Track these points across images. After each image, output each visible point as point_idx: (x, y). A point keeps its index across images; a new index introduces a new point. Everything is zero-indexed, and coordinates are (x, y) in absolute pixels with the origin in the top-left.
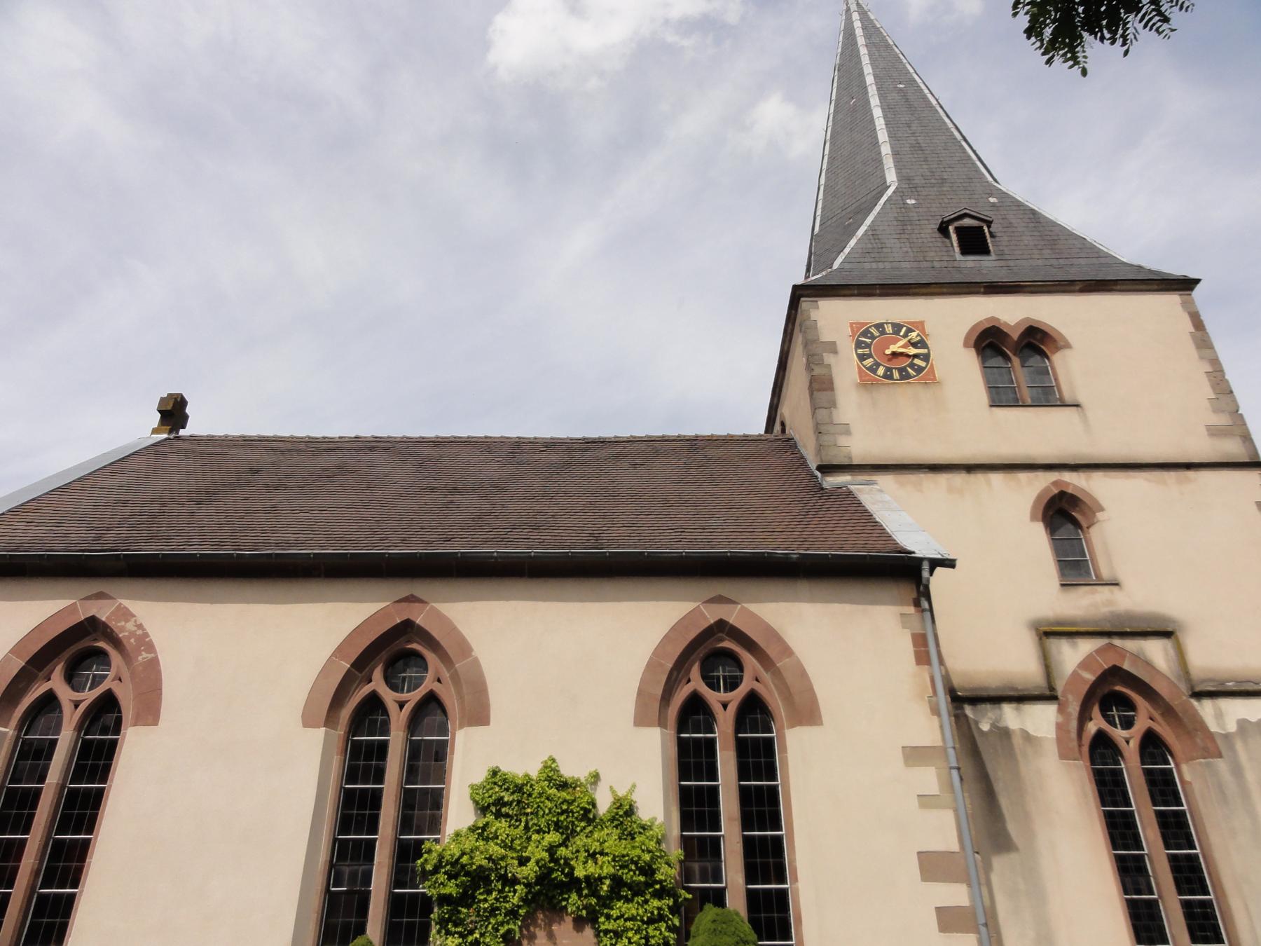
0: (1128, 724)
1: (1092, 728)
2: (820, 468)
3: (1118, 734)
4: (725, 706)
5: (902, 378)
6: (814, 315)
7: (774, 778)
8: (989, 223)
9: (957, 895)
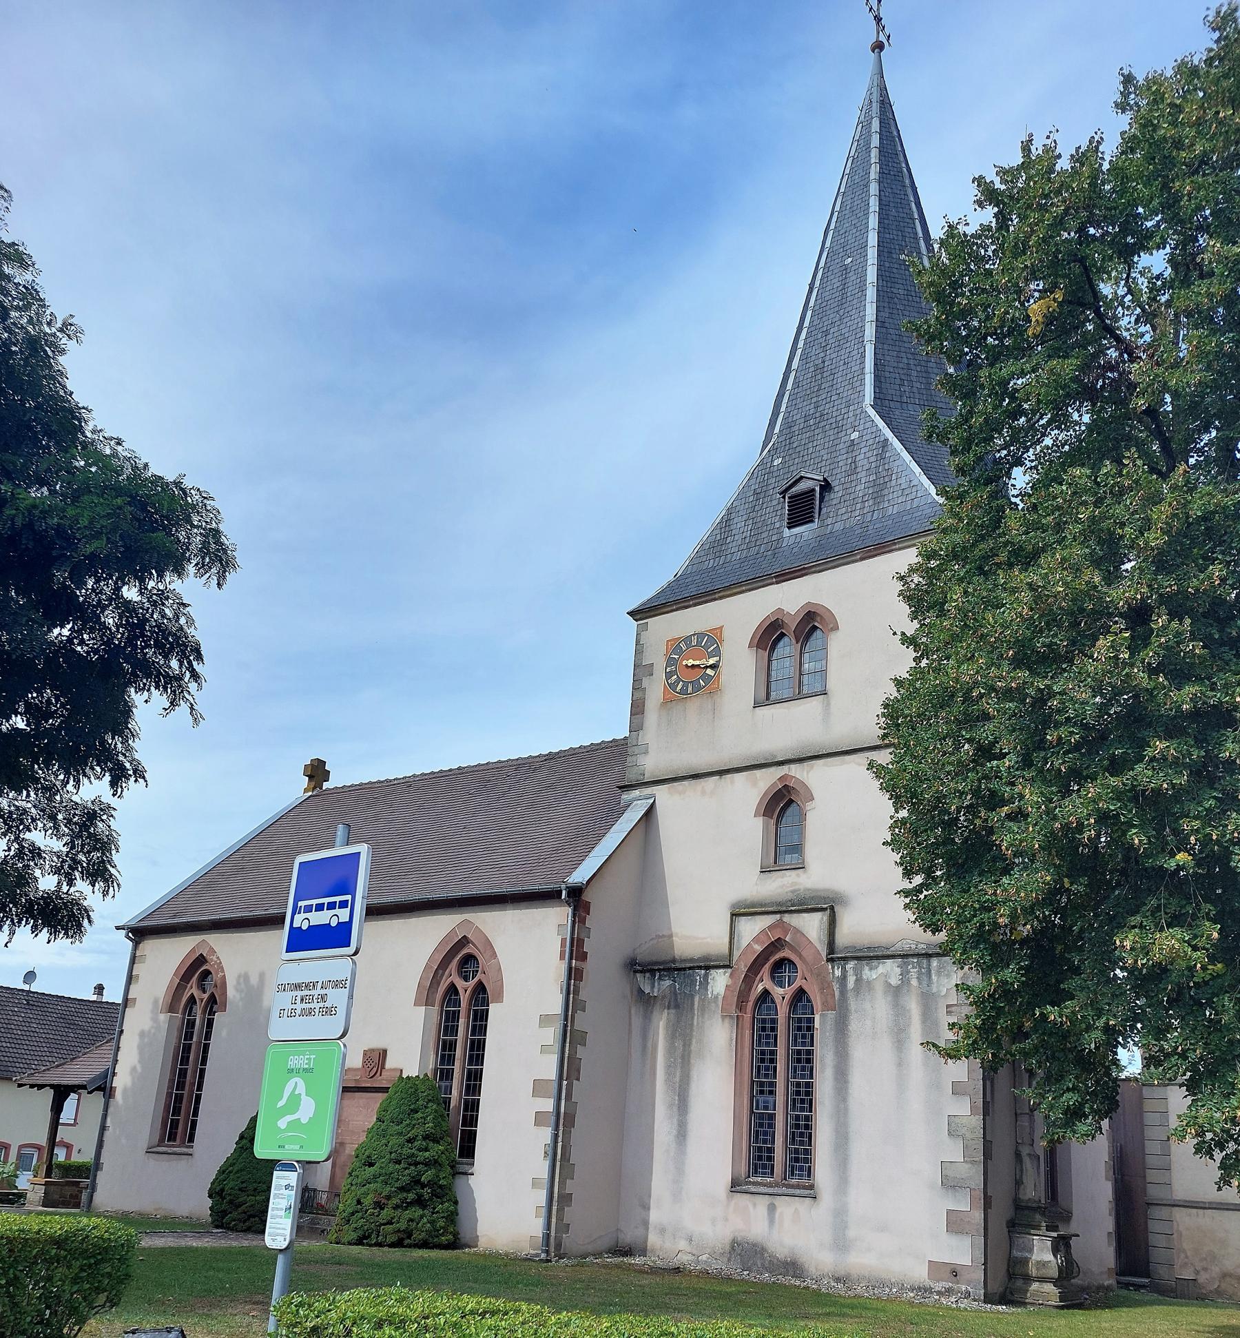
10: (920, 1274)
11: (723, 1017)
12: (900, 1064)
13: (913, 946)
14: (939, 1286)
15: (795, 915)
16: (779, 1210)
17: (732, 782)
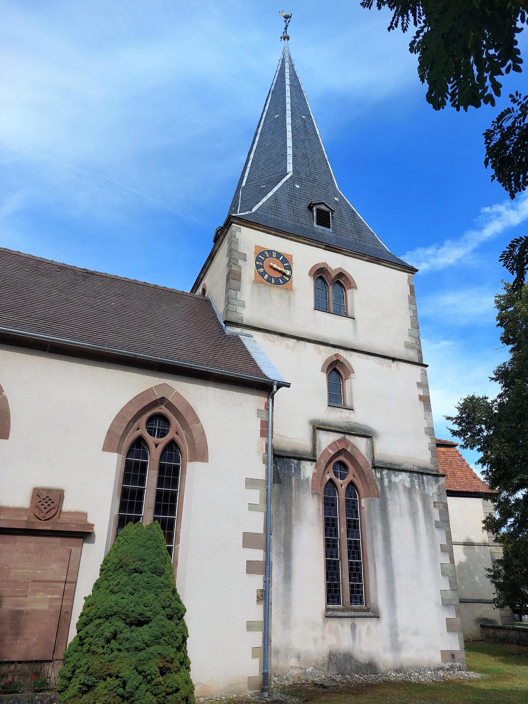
0: (343, 477)
1: (328, 477)
2: (225, 322)
3: (339, 481)
4: (156, 446)
5: (267, 280)
6: (238, 235)
7: (176, 487)
8: (333, 211)
9: (258, 555)
10: (437, 659)
11: (313, 494)
12: (416, 533)
13: (412, 467)
14: (447, 665)
15: (352, 437)
16: (358, 628)
17: (352, 355)
